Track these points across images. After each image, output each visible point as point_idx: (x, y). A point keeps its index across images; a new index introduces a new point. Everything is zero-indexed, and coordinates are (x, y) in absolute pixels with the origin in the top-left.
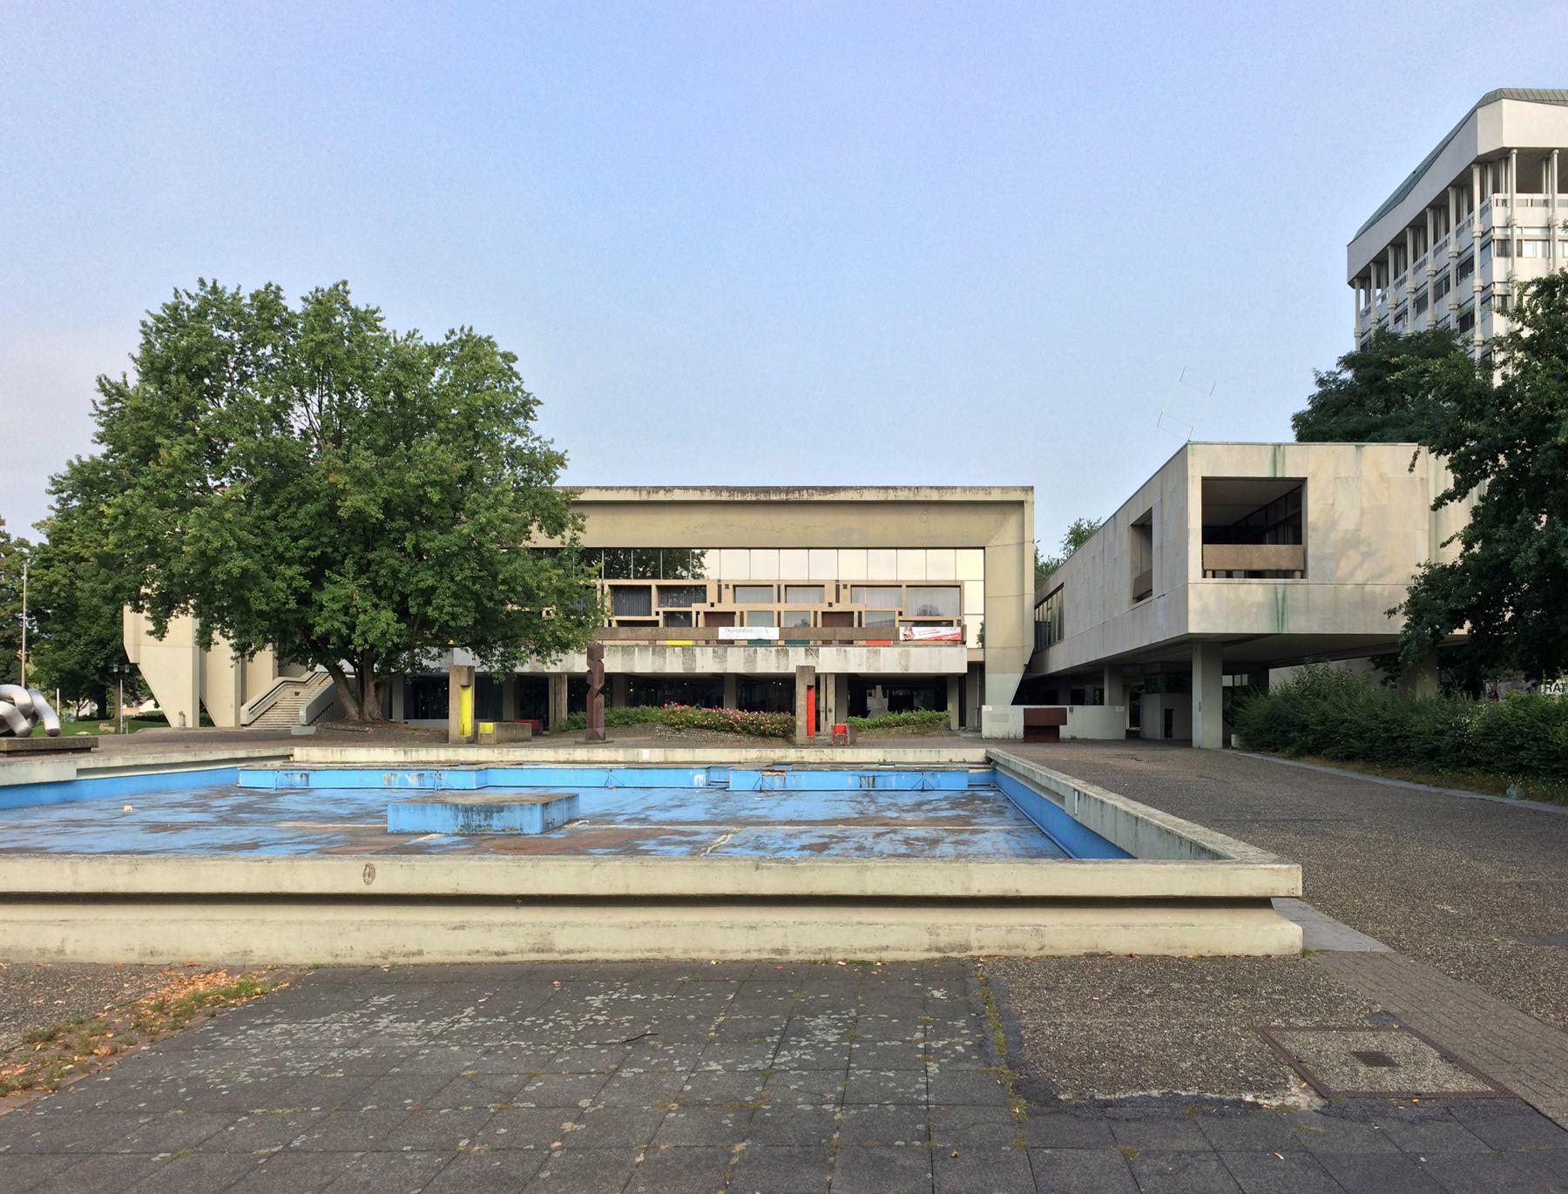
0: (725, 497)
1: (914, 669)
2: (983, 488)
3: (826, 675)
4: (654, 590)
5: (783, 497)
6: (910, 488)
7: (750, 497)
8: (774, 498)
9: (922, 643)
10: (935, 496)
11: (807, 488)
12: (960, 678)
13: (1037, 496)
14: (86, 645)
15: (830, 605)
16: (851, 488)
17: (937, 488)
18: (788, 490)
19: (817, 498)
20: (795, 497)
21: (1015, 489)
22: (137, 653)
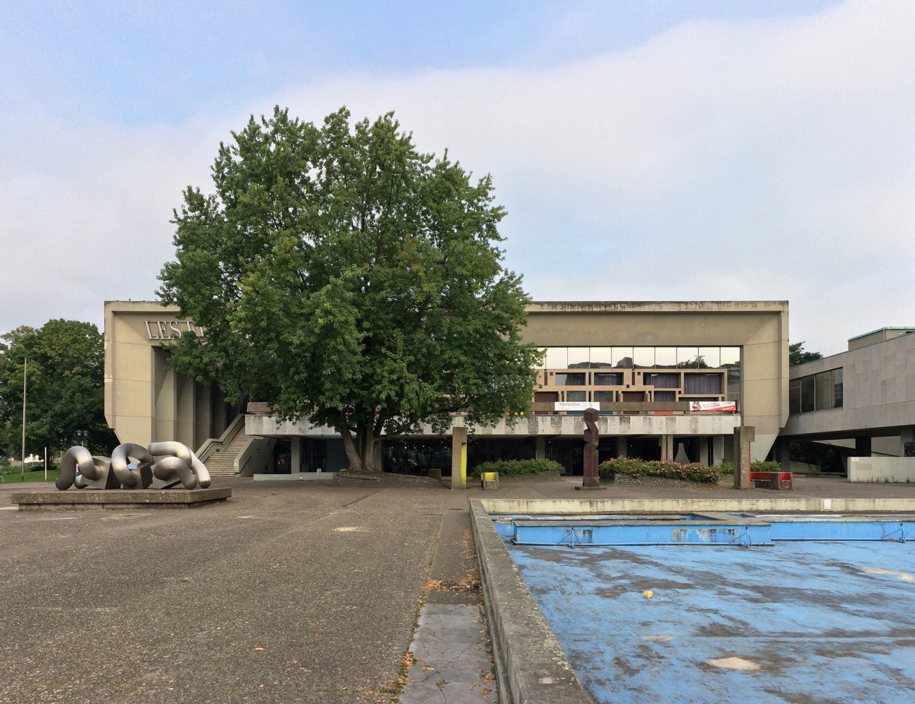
0: (559, 309)
1: (701, 431)
2: (751, 302)
3: (667, 435)
4: (682, 375)
5: (603, 309)
6: (696, 303)
7: (576, 309)
8: (595, 309)
9: (706, 413)
10: (715, 308)
11: (621, 303)
12: (727, 437)
13: (791, 308)
14: (52, 417)
15: (628, 386)
16: (654, 302)
17: (717, 302)
18: (606, 304)
19: (628, 309)
20: (612, 309)
21: (775, 302)
22: (114, 421)
